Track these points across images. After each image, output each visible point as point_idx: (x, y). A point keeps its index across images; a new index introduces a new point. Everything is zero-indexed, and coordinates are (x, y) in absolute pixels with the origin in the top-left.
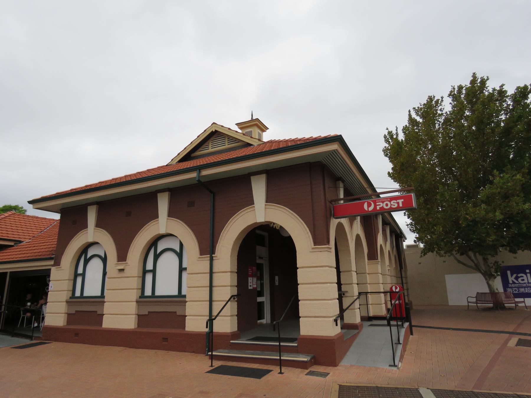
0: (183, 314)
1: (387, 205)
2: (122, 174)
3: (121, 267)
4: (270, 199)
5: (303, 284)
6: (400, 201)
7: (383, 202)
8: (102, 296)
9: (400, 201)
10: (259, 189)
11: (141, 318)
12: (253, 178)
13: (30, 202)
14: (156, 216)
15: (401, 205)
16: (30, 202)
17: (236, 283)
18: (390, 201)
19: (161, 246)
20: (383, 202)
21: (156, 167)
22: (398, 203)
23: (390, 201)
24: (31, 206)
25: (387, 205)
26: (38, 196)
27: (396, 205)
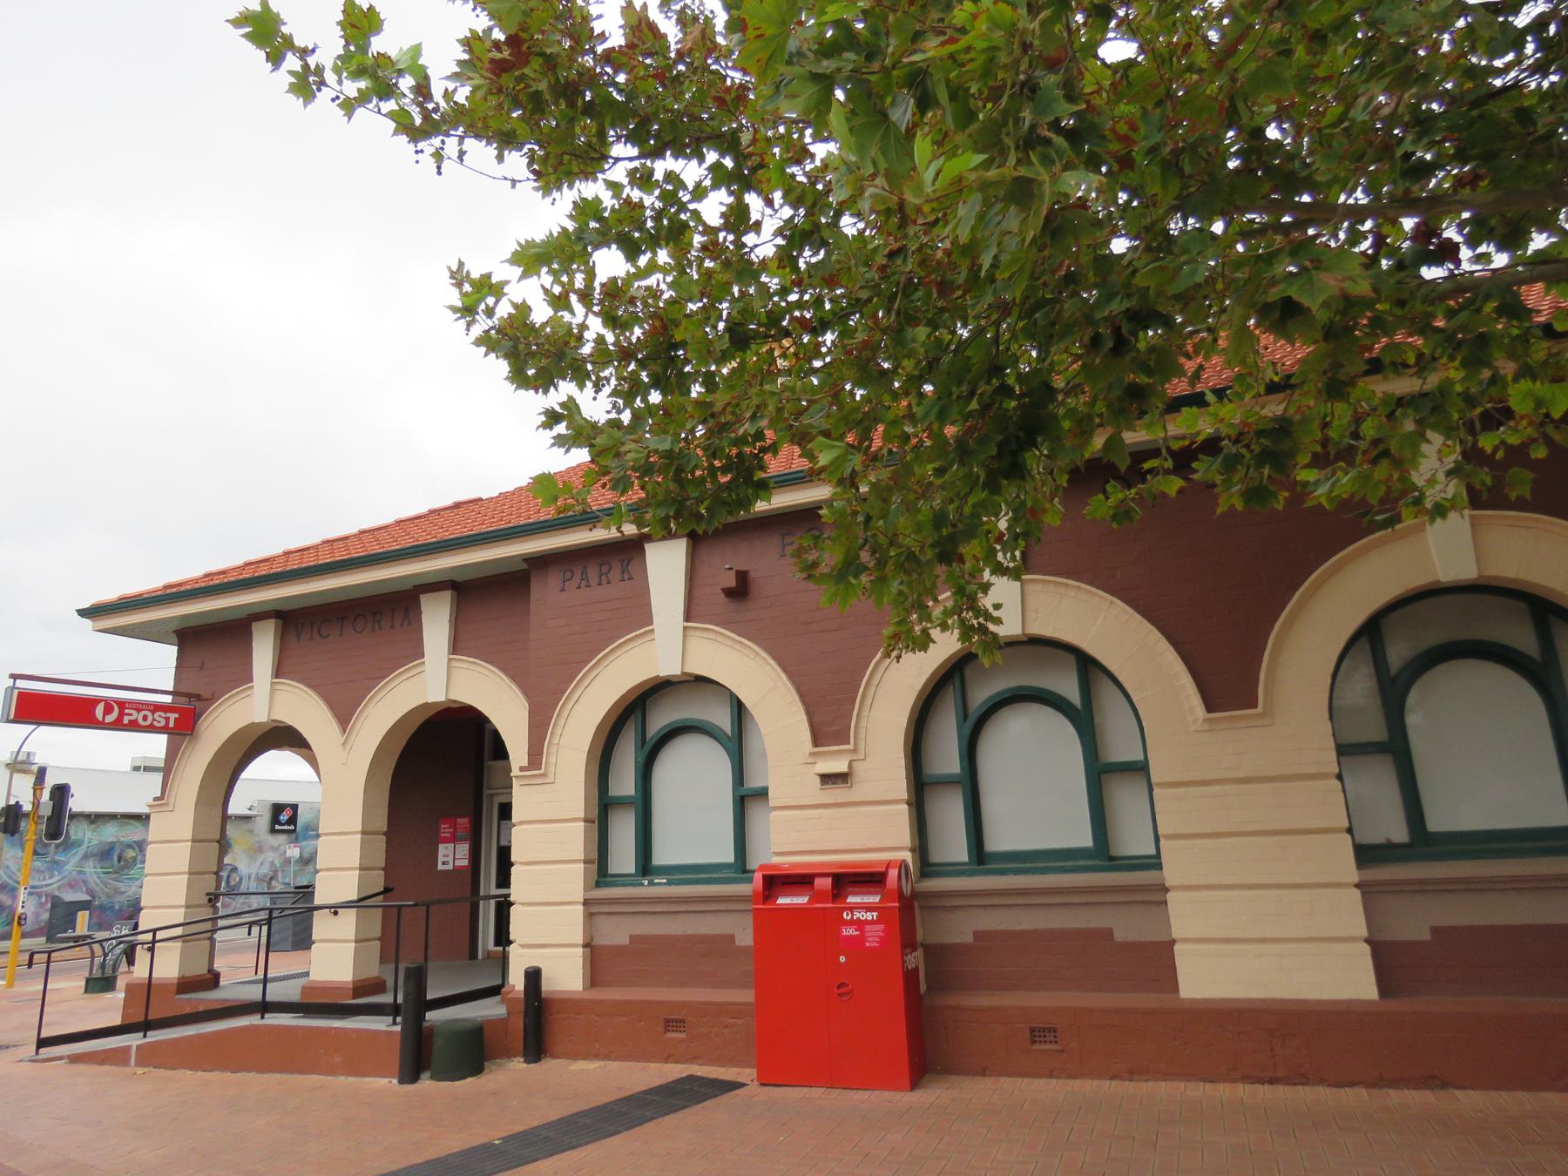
0: (1167, 939)
1: (145, 718)
2: (275, 549)
3: (840, 766)
4: (457, 646)
5: (1177, 888)
6: (173, 716)
7: (139, 711)
8: (1158, 855)
9: (173, 716)
10: (436, 622)
11: (1389, 959)
12: (423, 598)
13: (83, 613)
14: (415, 651)
15: (172, 724)
16: (83, 613)
17: (382, 823)
18: (153, 712)
19: (659, 720)
20: (139, 711)
21: (390, 520)
22: (167, 719)
23: (153, 712)
24: (88, 623)
25: (145, 718)
26: (110, 594)
27: (163, 723)
